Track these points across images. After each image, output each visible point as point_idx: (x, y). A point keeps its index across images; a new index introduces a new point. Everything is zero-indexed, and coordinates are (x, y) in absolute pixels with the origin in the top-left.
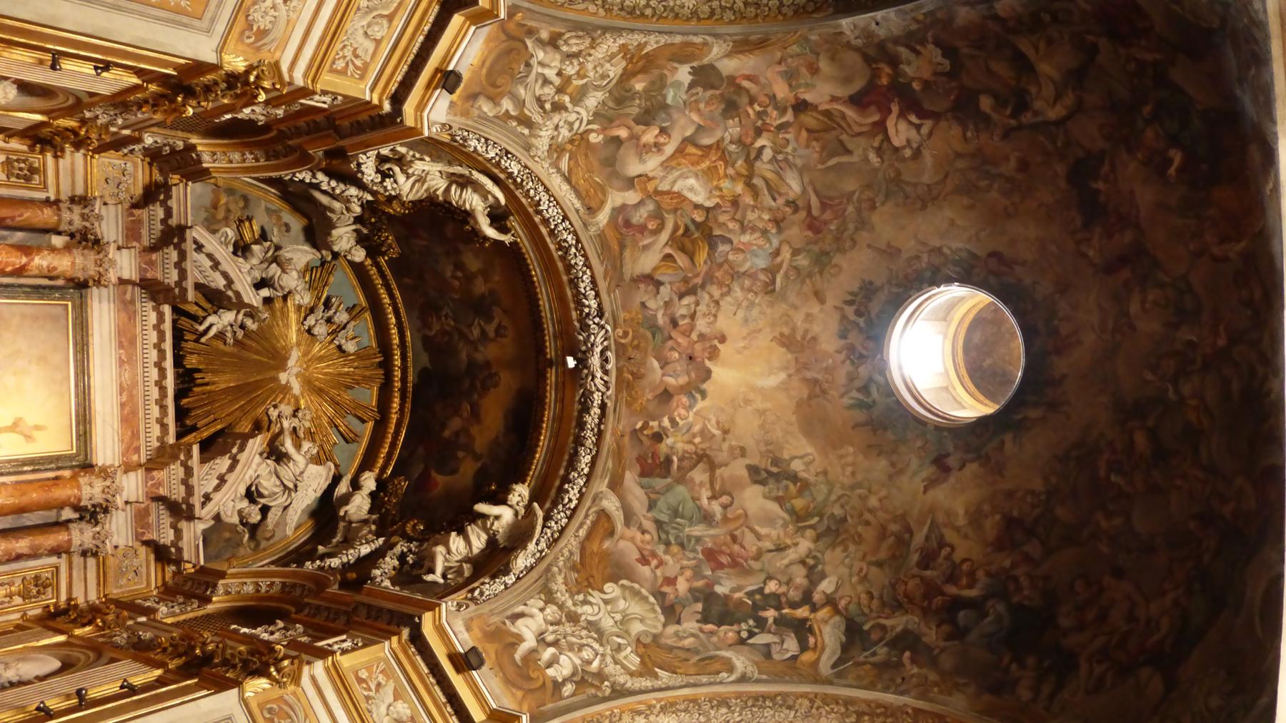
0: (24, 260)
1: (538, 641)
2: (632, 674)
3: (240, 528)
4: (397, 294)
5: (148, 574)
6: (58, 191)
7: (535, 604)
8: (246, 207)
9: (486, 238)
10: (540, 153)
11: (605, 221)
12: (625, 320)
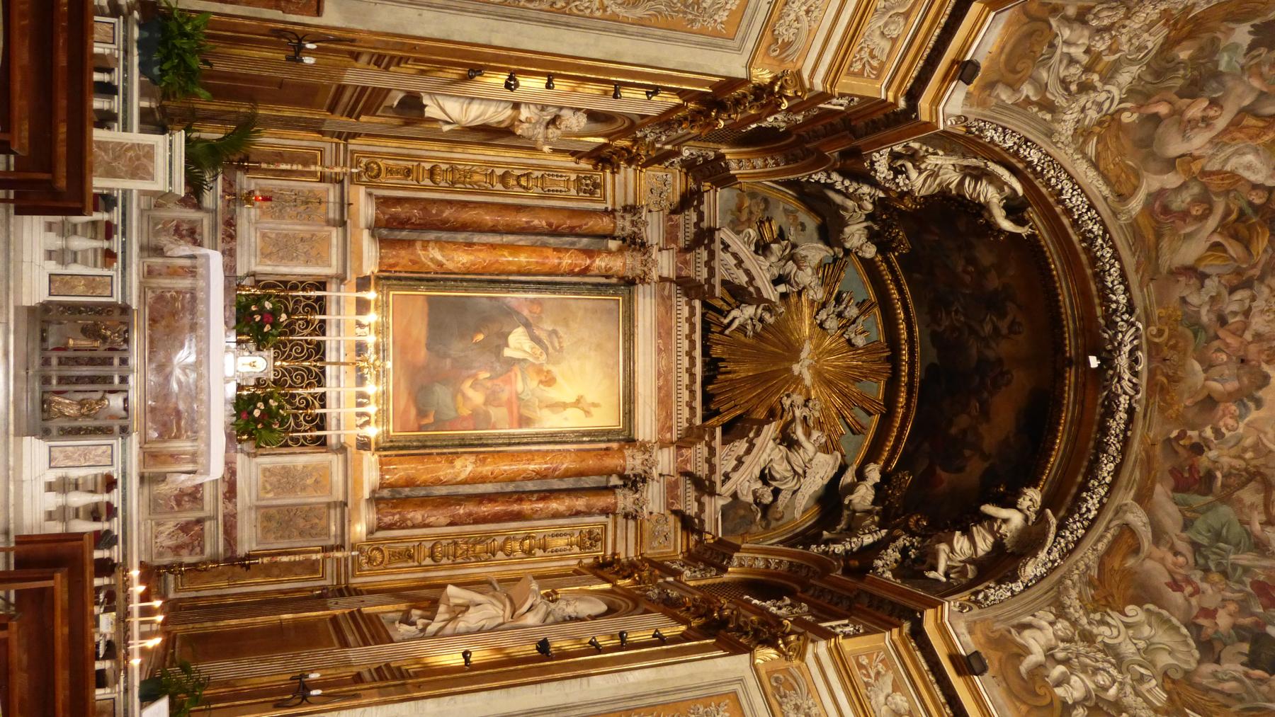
0: (588, 262)
4: (906, 289)
5: (676, 540)
7: (1044, 617)
8: (766, 209)
9: (1001, 231)
10: (1063, 139)
11: (1138, 208)
12: (1160, 318)
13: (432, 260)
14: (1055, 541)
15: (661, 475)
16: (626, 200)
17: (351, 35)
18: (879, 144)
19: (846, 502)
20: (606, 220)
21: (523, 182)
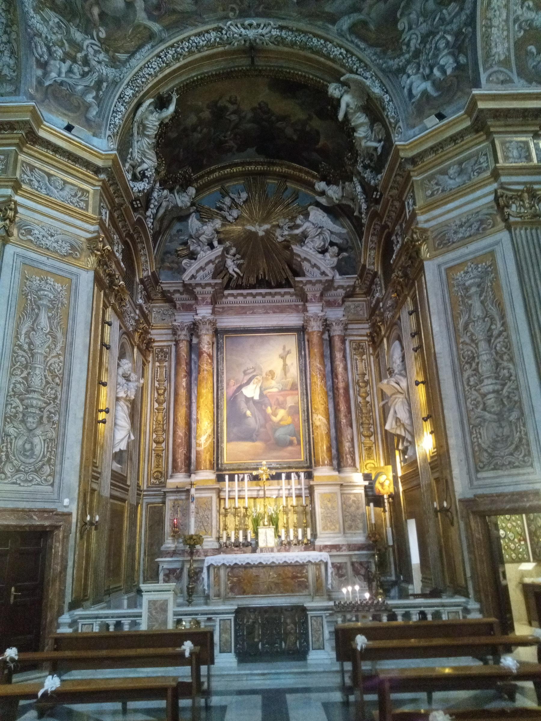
0: (205, 355)
1: (428, 79)
2: (462, 9)
3: (340, 257)
4: (213, 168)
5: (360, 301)
6: (171, 341)
7: (405, 81)
9: (176, 111)
10: (118, 75)
11: (158, 25)
12: (224, 10)
14: (360, 75)
15: (322, 311)
16: (169, 334)
18: (127, 189)
19: (337, 202)
20: (181, 345)
21: (161, 392)
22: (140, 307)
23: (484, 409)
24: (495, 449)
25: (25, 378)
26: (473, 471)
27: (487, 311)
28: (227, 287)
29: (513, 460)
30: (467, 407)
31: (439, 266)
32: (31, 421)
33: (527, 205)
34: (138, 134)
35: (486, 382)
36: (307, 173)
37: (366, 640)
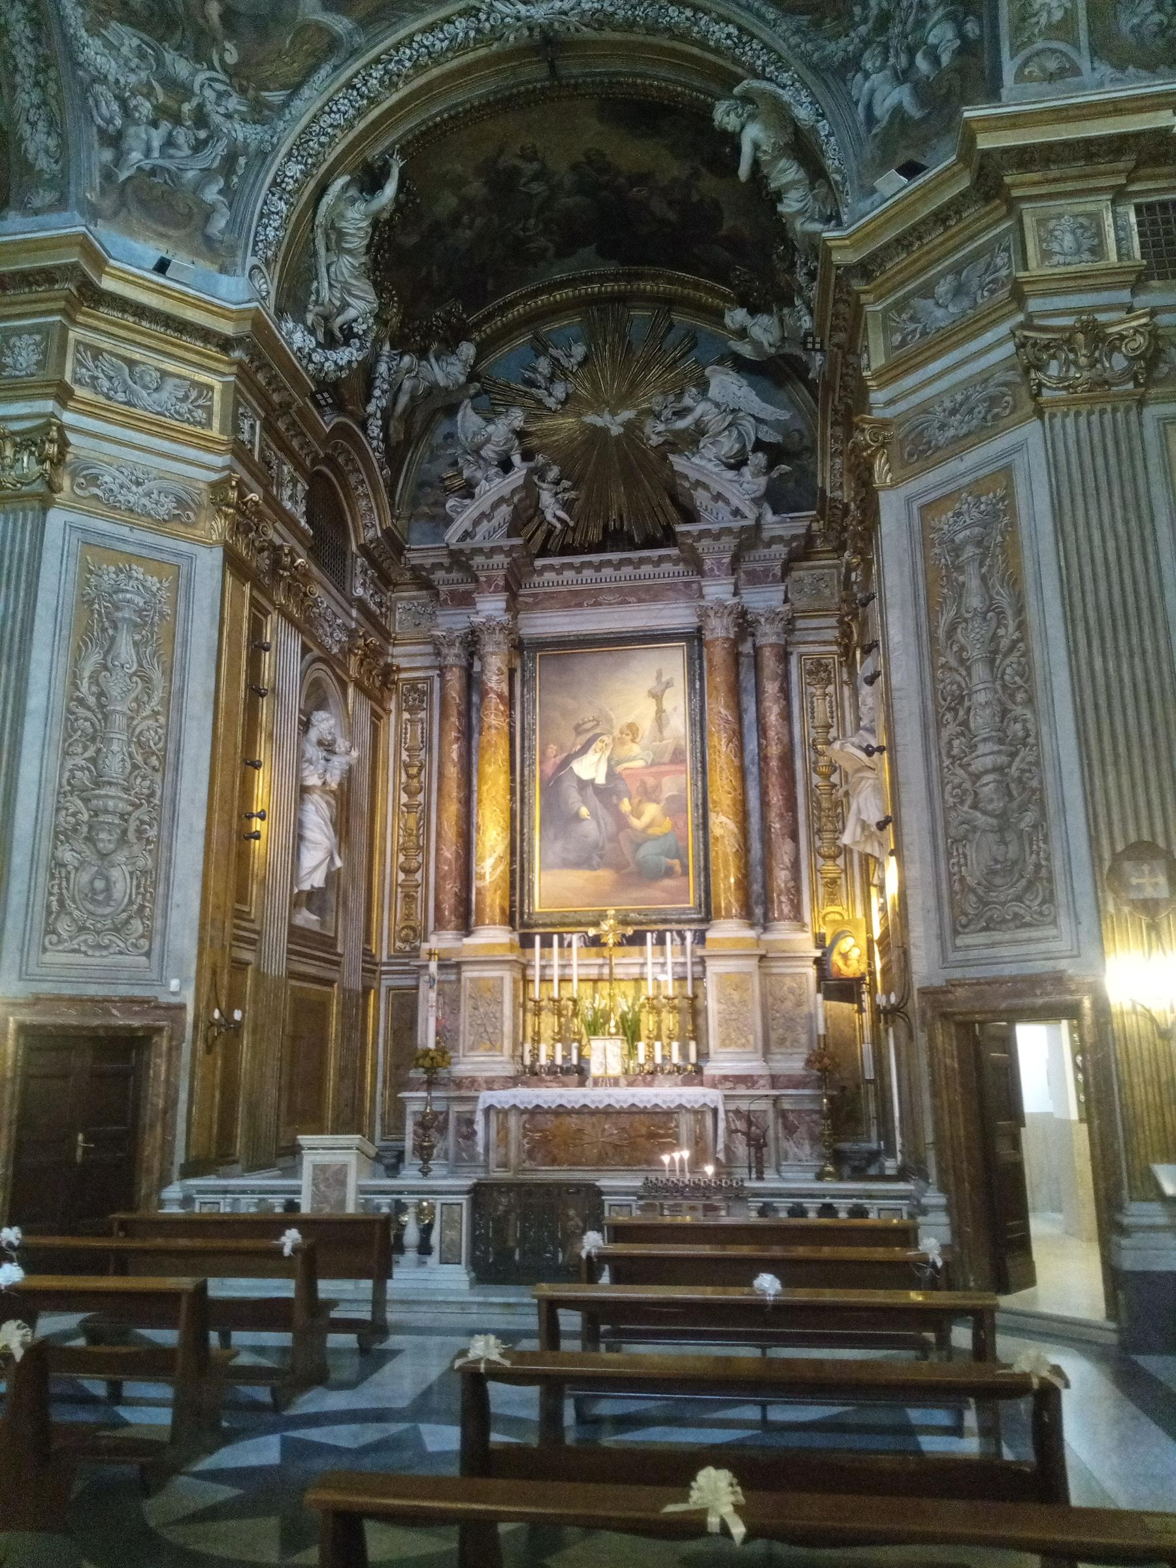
0: (492, 695)
5: (823, 567)
7: (860, 87)
8: (431, 485)
10: (267, 137)
11: (346, 21)
13: (494, 868)
14: (770, 80)
17: (208, 974)
19: (773, 350)
20: (449, 676)
22: (361, 604)
23: (975, 806)
24: (990, 887)
25: (93, 760)
26: (948, 932)
27: (992, 598)
28: (544, 552)
29: (1022, 912)
30: (944, 801)
31: (909, 501)
32: (106, 840)
33: (1083, 361)
34: (328, 250)
35: (982, 749)
36: (710, 291)
37: (601, 1243)
